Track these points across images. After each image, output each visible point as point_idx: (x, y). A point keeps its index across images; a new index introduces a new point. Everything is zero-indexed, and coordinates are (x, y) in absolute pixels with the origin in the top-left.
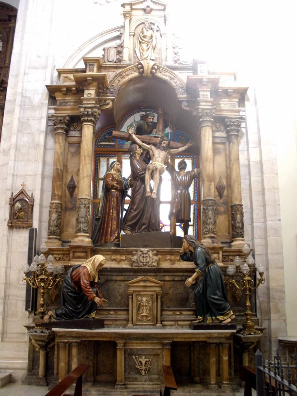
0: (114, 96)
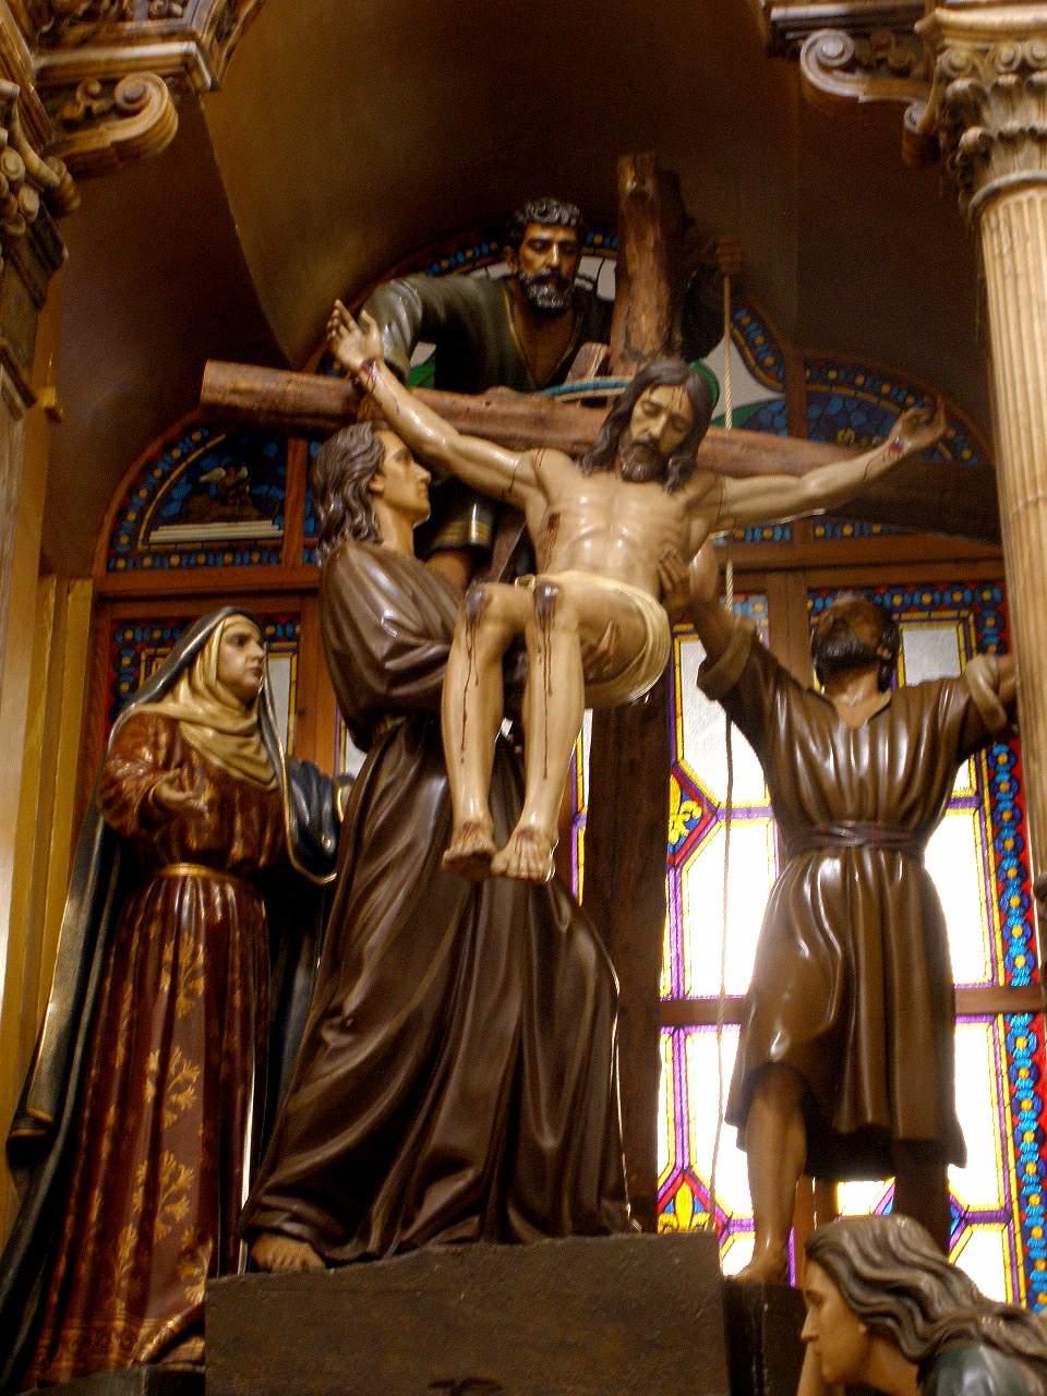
0: (189, 36)
